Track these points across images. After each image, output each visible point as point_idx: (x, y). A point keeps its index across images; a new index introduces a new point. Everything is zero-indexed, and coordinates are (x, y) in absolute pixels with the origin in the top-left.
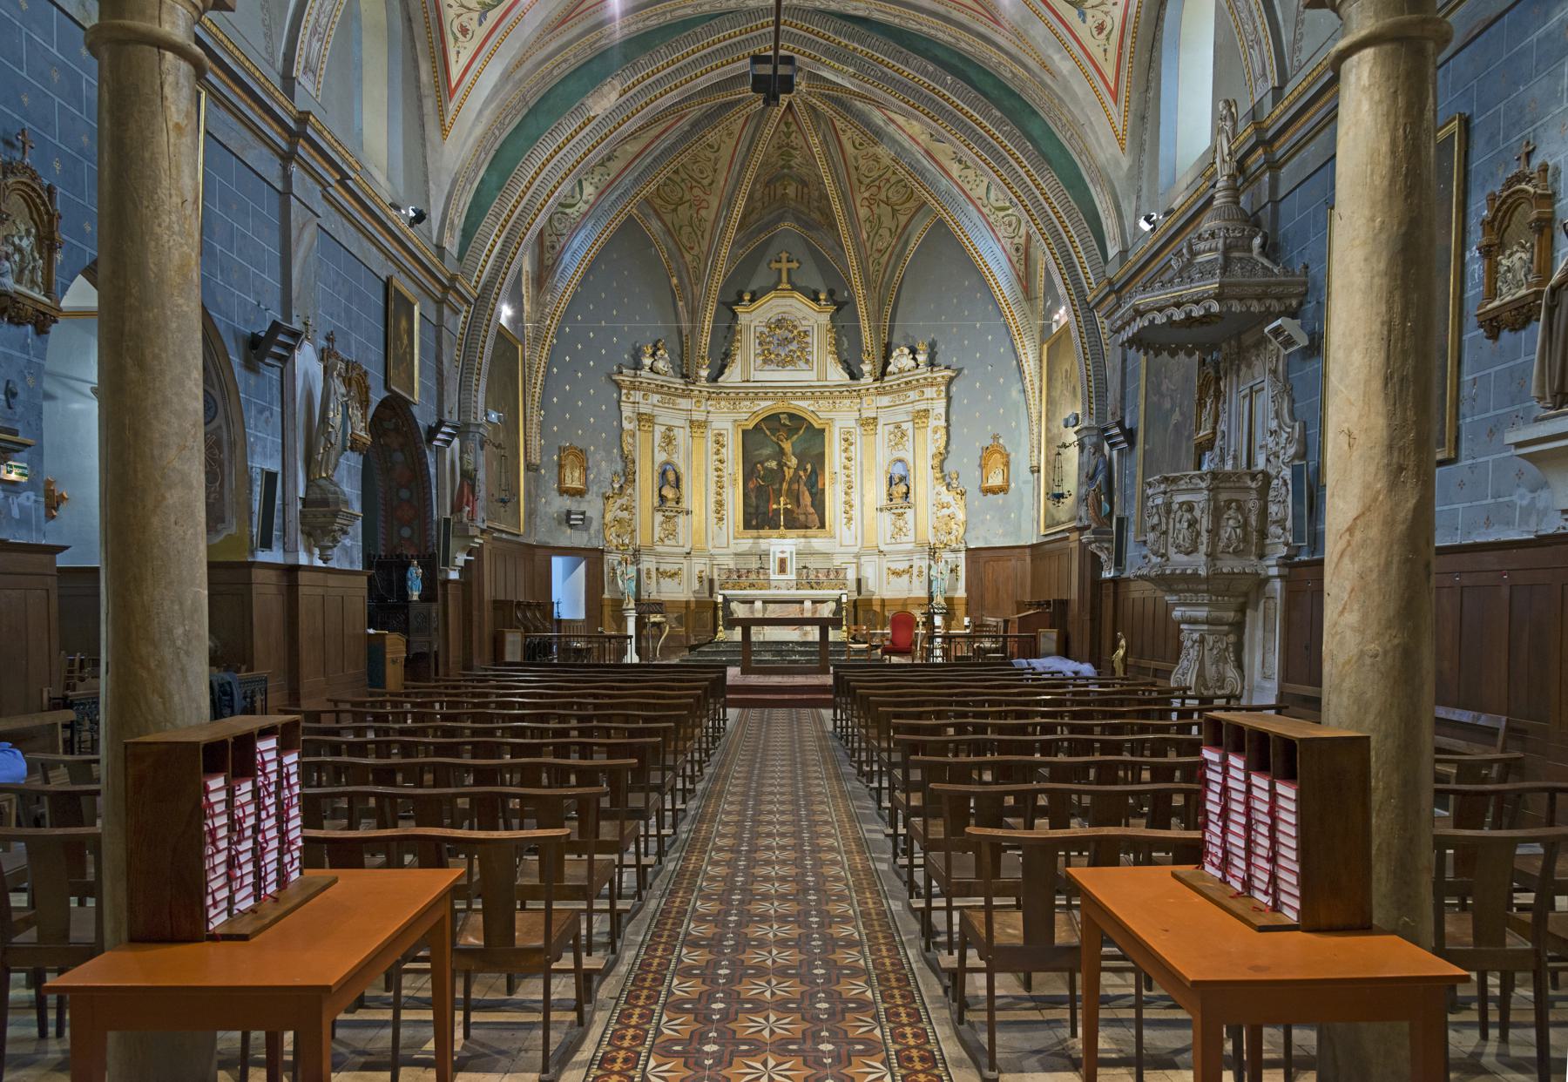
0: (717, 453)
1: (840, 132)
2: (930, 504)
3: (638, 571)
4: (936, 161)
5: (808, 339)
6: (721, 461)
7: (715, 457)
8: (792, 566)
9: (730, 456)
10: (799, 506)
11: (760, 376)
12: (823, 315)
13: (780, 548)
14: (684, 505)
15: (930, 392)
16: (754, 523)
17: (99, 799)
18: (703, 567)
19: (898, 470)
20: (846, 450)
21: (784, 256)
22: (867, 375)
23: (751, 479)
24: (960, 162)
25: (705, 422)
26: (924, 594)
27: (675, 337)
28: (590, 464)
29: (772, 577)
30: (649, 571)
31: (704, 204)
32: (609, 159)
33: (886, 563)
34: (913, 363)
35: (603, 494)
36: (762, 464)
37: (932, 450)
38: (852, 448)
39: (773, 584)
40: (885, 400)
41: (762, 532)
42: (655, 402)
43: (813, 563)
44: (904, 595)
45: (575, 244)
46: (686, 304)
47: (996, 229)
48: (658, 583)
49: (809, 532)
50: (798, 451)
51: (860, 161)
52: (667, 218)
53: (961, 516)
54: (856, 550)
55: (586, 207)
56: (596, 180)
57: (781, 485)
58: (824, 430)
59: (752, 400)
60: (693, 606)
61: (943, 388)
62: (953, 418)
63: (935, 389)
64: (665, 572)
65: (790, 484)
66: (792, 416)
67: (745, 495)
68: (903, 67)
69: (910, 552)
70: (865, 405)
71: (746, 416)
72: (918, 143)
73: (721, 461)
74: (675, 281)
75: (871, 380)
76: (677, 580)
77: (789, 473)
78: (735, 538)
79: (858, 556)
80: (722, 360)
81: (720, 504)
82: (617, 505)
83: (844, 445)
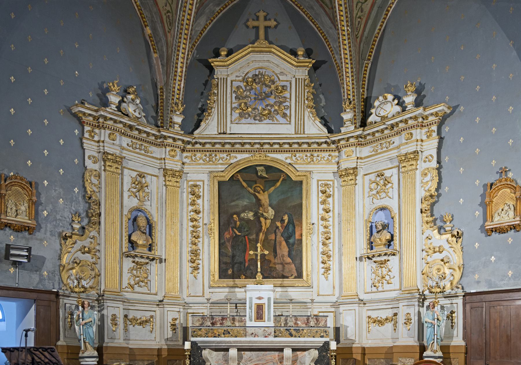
0: (193, 204)
2: (419, 250)
3: (102, 318)
5: (287, 94)
6: (197, 212)
7: (191, 208)
8: (269, 313)
9: (206, 207)
10: (275, 256)
11: (236, 129)
12: (301, 70)
13: (258, 294)
14: (159, 251)
15: (419, 134)
16: (230, 272)
17: (328, 318)
18: (176, 316)
19: (381, 218)
20: (324, 202)
21: (262, 14)
22: (348, 123)
23: (227, 229)
25: (181, 171)
26: (412, 341)
27: (149, 87)
28: (43, 199)
29: (248, 324)
30: (114, 318)
33: (365, 312)
34: (398, 109)
35: (60, 234)
36: (238, 214)
37: (420, 193)
38: (330, 200)
39: (250, 331)
40: (366, 151)
41: (238, 281)
42: (125, 145)
43: (291, 310)
44: (389, 343)
46: (161, 57)
48: (126, 330)
49: (286, 282)
50: (275, 203)
53: (456, 259)
54: (334, 299)
57: (258, 235)
58: (301, 182)
59: (229, 151)
60: (165, 354)
61: (434, 128)
62: (445, 159)
63: (425, 130)
64: (135, 319)
65: (267, 234)
66: (269, 169)
67: (221, 245)
69: (397, 300)
70: (344, 156)
71: (221, 168)
73: (197, 212)
74: (148, 31)
75: (352, 128)
76: (148, 327)
77: (265, 224)
78: (210, 287)
79: (336, 305)
80: (199, 115)
81: (195, 253)
82: (77, 246)
83: (322, 197)
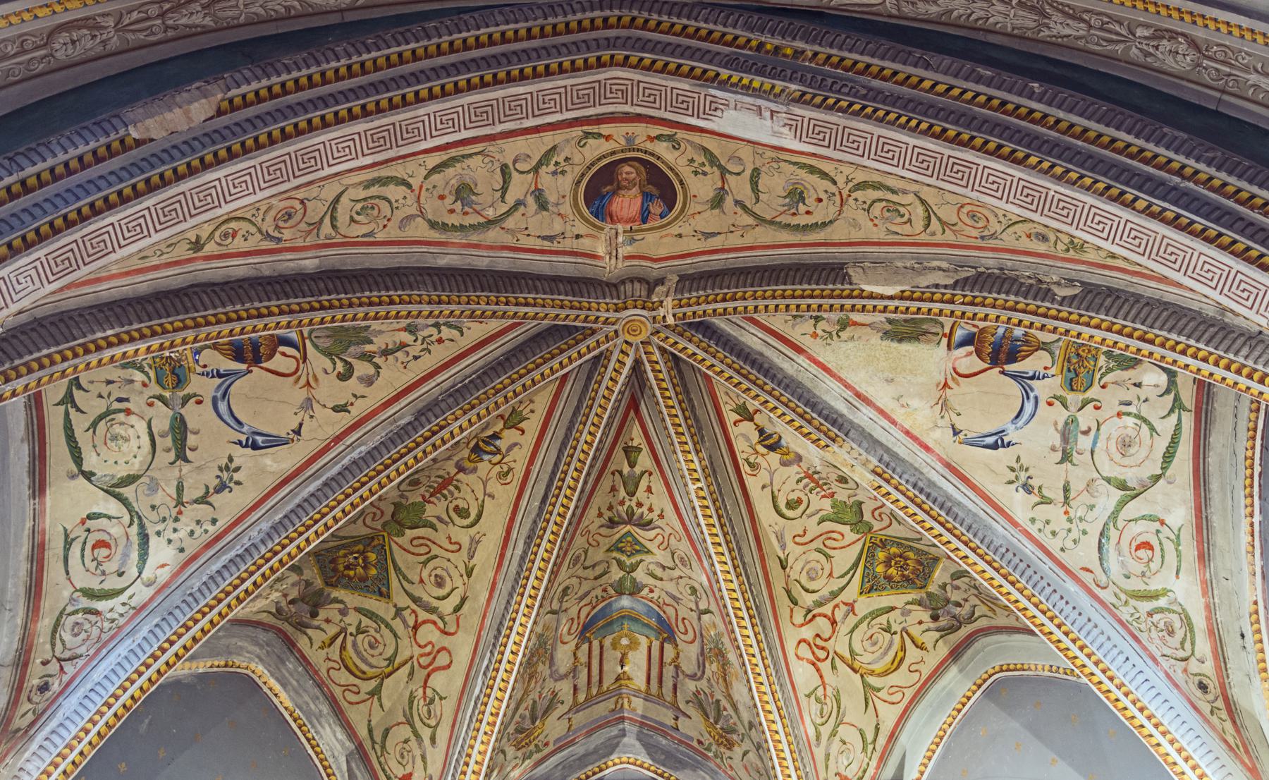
1: (745, 468)
4: (973, 487)
24: (1028, 488)
31: (442, 659)
32: (221, 488)
45: (97, 676)
47: (1143, 637)
51: (790, 546)
52: (357, 717)
55: (148, 592)
56: (182, 534)
68: (921, 72)
72: (927, 448)
